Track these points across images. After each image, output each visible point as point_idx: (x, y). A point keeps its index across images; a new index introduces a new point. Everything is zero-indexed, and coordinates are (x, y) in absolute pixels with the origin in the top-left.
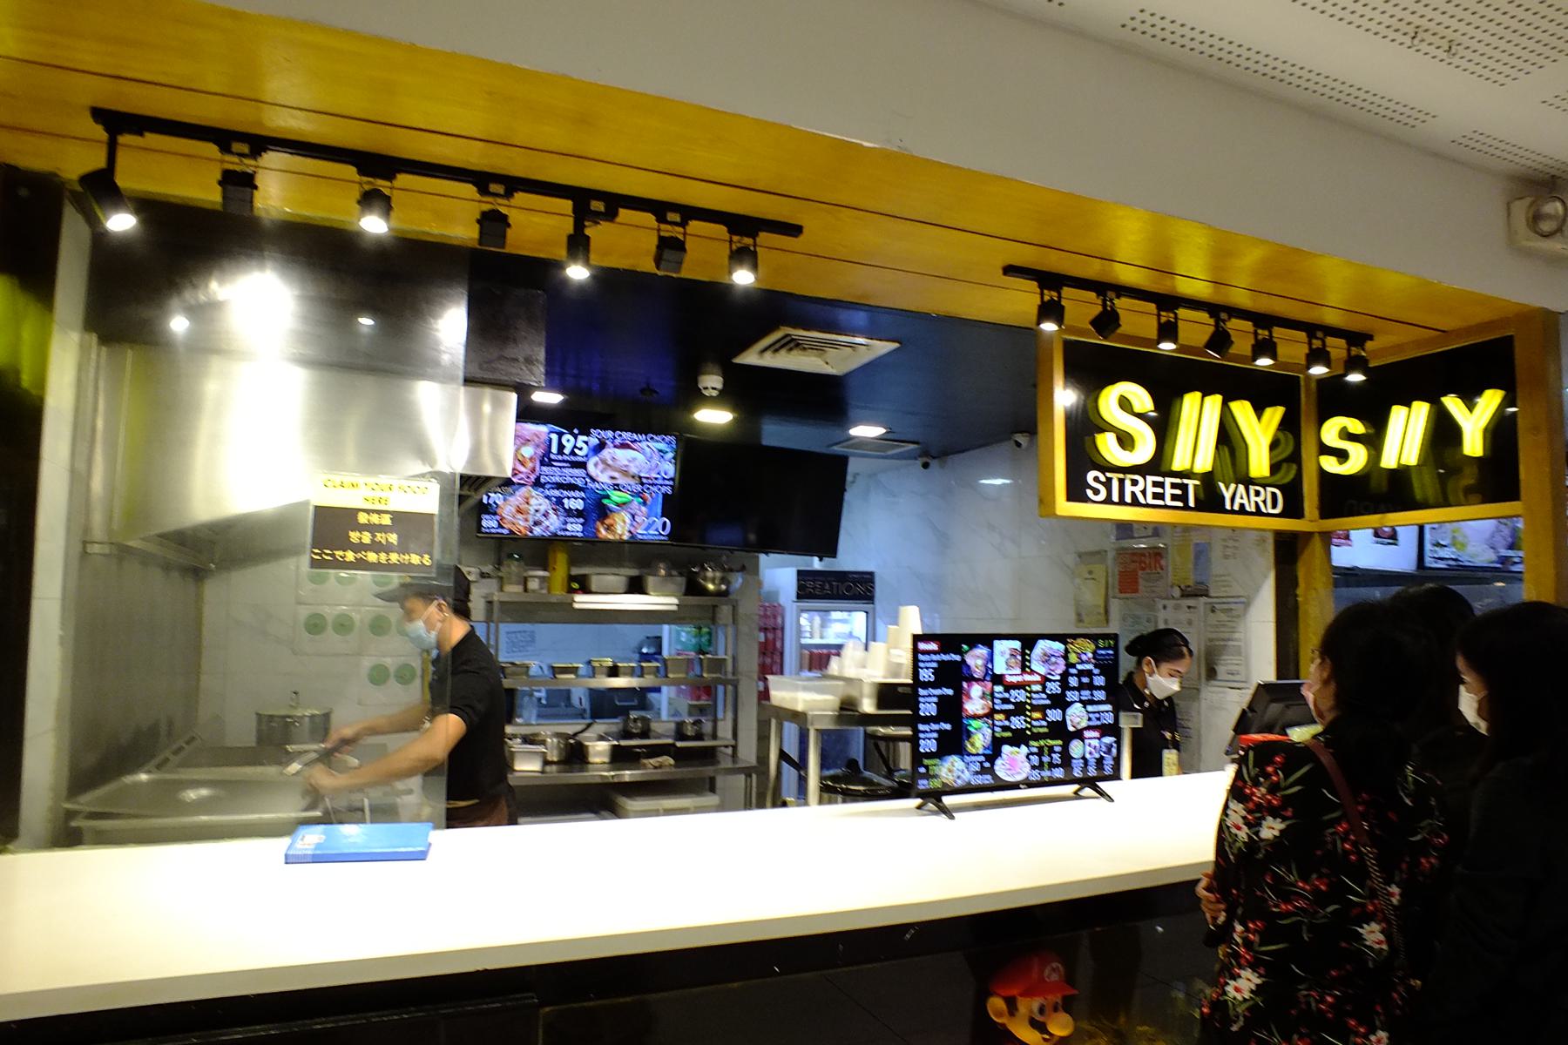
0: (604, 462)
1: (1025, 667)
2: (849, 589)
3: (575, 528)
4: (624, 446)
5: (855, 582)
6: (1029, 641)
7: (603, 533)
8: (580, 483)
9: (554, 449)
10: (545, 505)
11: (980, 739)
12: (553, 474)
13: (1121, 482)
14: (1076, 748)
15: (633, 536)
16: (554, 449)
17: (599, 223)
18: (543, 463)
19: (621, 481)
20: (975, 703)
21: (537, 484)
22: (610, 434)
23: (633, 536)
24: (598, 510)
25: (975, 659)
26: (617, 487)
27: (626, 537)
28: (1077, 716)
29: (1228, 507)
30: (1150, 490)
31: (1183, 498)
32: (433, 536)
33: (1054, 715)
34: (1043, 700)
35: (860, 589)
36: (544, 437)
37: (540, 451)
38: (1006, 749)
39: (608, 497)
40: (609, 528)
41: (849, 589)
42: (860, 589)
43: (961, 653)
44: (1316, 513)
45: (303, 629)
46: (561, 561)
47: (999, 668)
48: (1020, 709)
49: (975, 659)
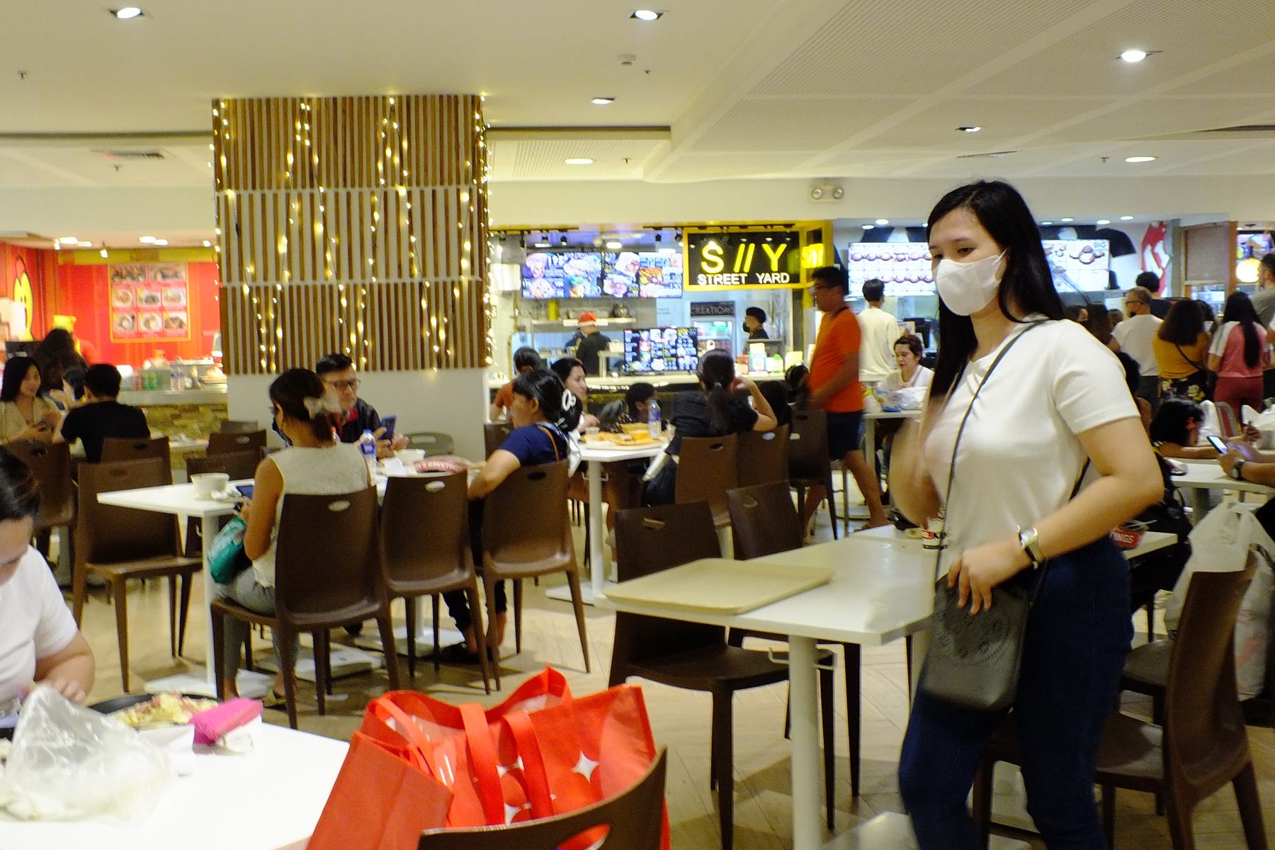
0: (571, 266)
1: (662, 337)
2: (720, 310)
3: (561, 294)
4: (579, 258)
5: (723, 306)
6: (663, 330)
7: (572, 295)
8: (561, 275)
9: (550, 262)
10: (548, 285)
11: (646, 357)
12: (550, 273)
13: (713, 278)
14: (681, 361)
15: (585, 295)
16: (550, 262)
17: (363, 408)
18: (546, 268)
19: (579, 273)
20: (644, 347)
21: (544, 277)
22: (572, 254)
23: (585, 295)
24: (569, 285)
25: (644, 335)
26: (577, 276)
27: (582, 296)
28: (681, 351)
29: (761, 281)
30: (725, 279)
31: (740, 281)
32: (743, 233)
33: (673, 351)
34: (669, 347)
35: (727, 310)
36: (546, 259)
37: (545, 264)
38: (655, 360)
39: (573, 280)
40: (575, 293)
41: (720, 310)
42: (727, 310)
43: (639, 333)
44: (805, 281)
45: (949, 567)
46: (552, 307)
47: (653, 338)
48: (660, 349)
49: (644, 335)
